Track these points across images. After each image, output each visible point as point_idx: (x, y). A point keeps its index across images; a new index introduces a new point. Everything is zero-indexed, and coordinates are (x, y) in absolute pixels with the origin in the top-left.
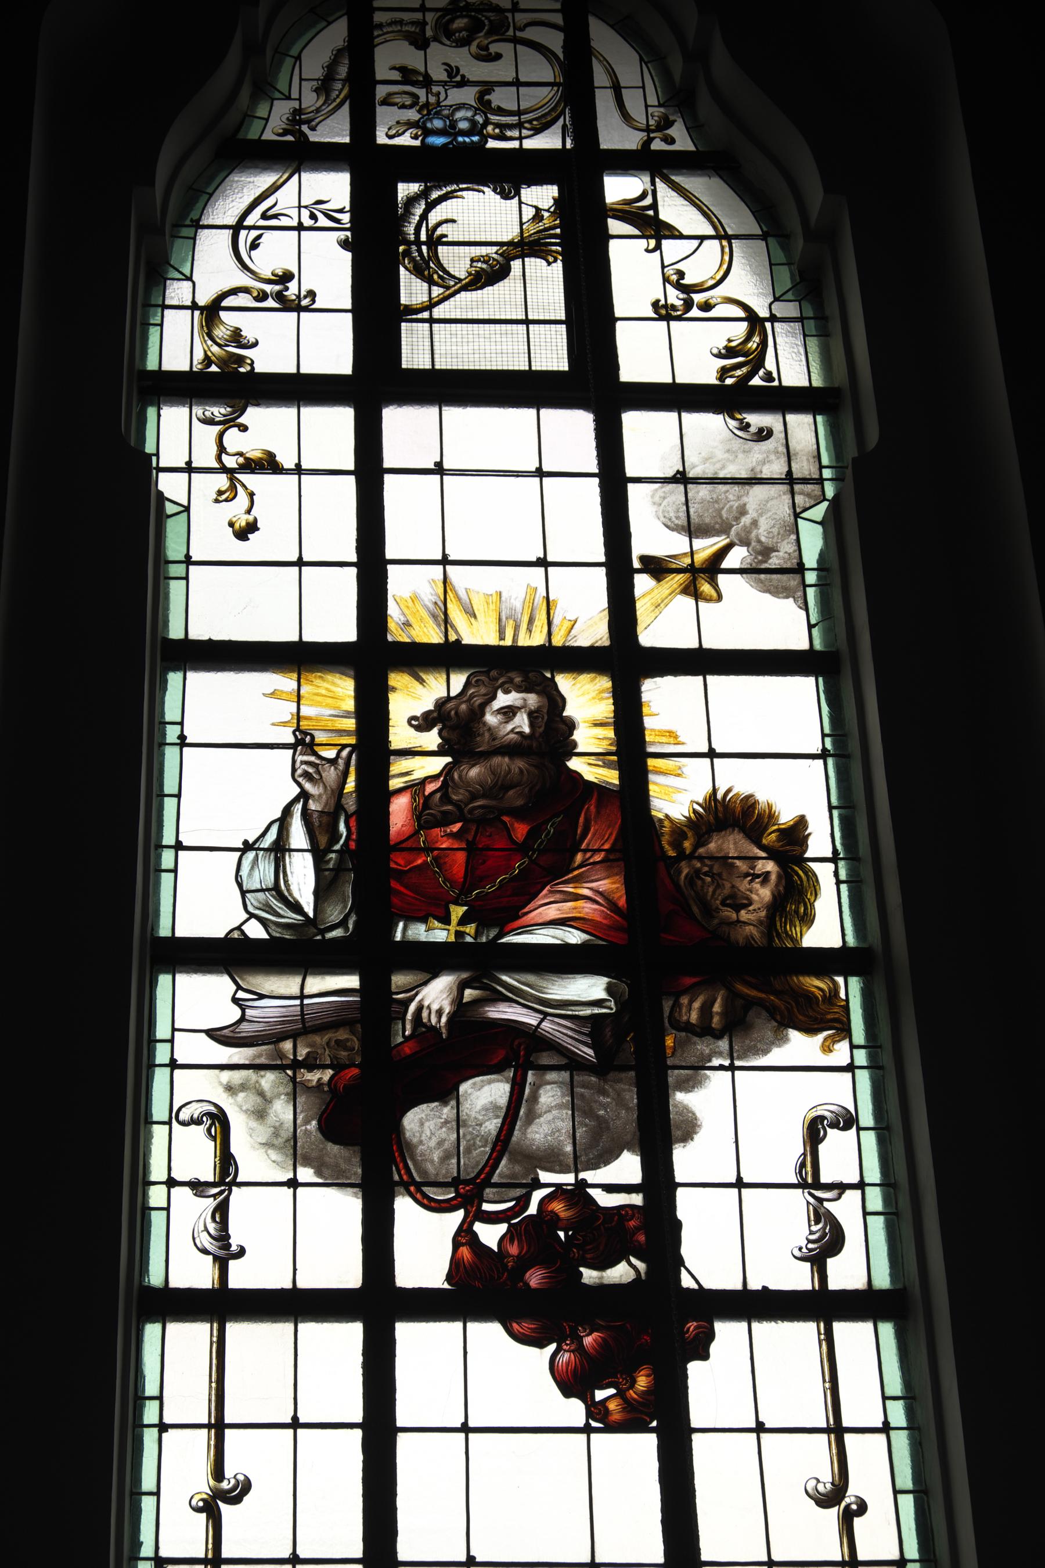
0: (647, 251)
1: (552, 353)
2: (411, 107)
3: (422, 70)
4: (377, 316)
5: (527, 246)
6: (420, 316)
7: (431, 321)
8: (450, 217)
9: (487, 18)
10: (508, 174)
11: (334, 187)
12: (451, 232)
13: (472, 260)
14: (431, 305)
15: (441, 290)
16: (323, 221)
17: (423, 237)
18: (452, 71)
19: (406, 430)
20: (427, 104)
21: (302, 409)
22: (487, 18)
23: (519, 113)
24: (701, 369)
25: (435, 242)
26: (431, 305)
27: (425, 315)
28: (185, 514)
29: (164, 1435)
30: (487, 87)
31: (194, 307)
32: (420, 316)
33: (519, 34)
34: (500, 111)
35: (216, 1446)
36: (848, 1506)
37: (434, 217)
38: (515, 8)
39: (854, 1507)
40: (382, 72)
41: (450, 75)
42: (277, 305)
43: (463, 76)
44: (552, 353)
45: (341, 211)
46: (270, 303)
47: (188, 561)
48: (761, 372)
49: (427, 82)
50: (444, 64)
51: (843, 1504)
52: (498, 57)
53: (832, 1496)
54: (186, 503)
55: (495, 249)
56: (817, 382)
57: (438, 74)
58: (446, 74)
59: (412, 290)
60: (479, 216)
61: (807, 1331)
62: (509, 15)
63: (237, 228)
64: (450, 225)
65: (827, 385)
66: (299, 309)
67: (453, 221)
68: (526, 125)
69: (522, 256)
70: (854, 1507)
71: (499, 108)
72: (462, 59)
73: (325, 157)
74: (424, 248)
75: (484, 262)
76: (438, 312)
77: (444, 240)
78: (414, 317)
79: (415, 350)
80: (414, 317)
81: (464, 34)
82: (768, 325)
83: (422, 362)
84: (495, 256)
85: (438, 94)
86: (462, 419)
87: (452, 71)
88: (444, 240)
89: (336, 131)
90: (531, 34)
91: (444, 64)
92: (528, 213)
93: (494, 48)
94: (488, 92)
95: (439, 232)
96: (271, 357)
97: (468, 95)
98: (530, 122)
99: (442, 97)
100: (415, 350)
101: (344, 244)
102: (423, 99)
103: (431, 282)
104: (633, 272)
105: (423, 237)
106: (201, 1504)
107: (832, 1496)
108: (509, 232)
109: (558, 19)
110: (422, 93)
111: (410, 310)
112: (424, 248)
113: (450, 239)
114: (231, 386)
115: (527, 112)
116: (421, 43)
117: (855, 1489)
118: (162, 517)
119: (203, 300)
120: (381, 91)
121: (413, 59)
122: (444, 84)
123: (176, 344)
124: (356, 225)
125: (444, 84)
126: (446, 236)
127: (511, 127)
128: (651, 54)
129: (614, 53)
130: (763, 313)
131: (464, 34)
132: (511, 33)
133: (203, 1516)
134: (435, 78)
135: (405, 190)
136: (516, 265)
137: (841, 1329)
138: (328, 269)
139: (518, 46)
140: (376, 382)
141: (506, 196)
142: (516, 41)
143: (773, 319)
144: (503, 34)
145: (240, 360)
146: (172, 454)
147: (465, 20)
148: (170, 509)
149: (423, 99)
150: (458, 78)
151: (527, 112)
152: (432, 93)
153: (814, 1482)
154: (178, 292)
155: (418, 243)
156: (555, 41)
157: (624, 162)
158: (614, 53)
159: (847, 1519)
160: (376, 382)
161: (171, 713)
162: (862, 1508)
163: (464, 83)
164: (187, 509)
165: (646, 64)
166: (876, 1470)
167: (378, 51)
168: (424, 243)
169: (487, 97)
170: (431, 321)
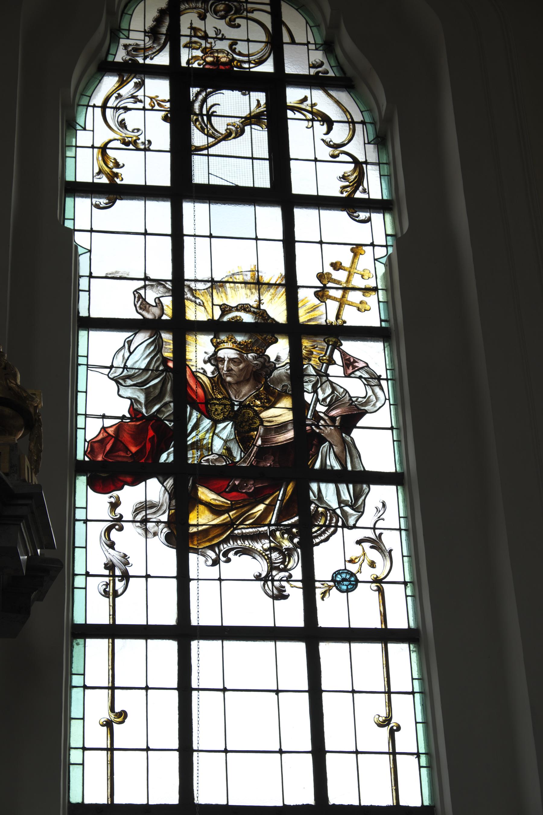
0: (307, 127)
1: (263, 180)
2: (197, 49)
3: (203, 29)
4: (182, 154)
5: (251, 119)
6: (201, 152)
7: (208, 155)
8: (217, 103)
9: (234, 5)
10: (245, 82)
11: (159, 88)
12: (218, 110)
13: (228, 125)
14: (208, 147)
15: (214, 140)
16: (157, 107)
17: (204, 112)
18: (218, 31)
19: (195, 213)
20: (206, 48)
21: (147, 202)
22: (234, 5)
23: (248, 56)
24: (332, 188)
25: (210, 116)
26: (208, 147)
27: (205, 152)
28: (89, 253)
29: (371, 241)
30: (234, 42)
31: (93, 147)
32: (201, 152)
33: (250, 15)
34: (240, 54)
35: (112, 695)
36: (392, 727)
37: (211, 101)
38: (247, 2)
39: (395, 728)
40: (185, 30)
41: (216, 34)
42: (134, 148)
43: (223, 35)
44: (263, 180)
45: (164, 101)
46: (131, 147)
47: (91, 276)
48: (361, 188)
49: (205, 37)
50: (215, 27)
51: (391, 726)
52: (239, 26)
53: (386, 722)
54: (89, 249)
55: (238, 119)
56: (385, 198)
57: (211, 33)
58: (214, 33)
59: (198, 138)
60: (231, 104)
61: (377, 647)
62: (245, 4)
63: (104, 107)
64: (217, 106)
65: (389, 198)
66: (146, 150)
67: (219, 105)
68: (252, 62)
69: (250, 124)
70: (395, 728)
71: (240, 52)
72: (222, 24)
73: (157, 72)
74: (205, 118)
75: (234, 126)
76: (212, 151)
77: (215, 114)
78: (199, 153)
79: (201, 172)
80: (199, 153)
81: (223, 13)
82: (364, 166)
83: (96, 796)
84: (238, 123)
85: (211, 43)
86: (222, 211)
87: (218, 31)
88: (215, 114)
89: (163, 59)
90: (256, 15)
91: (215, 27)
92: (254, 104)
93: (238, 21)
94: (236, 44)
95: (212, 110)
96: (130, 176)
97: (224, 45)
98: (254, 61)
99: (213, 44)
100: (201, 172)
101: (165, 119)
102: (203, 46)
103: (208, 135)
104: (301, 137)
105: (204, 112)
106: (105, 723)
107: (386, 722)
108: (245, 113)
109: (268, 8)
110: (203, 42)
111: (199, 149)
112: (205, 118)
113: (217, 114)
114: (113, 191)
115: (253, 55)
116: (202, 17)
117: (395, 720)
118: (77, 255)
119: (98, 144)
120: (184, 41)
121: (198, 24)
122: (213, 38)
123: (83, 167)
124: (172, 110)
125: (213, 38)
126: (216, 112)
127: (245, 62)
128: (313, 22)
129: (294, 21)
130: (361, 159)
131: (223, 13)
132: (245, 13)
133: (105, 728)
134: (210, 36)
135: (194, 91)
136: (247, 128)
137: (391, 646)
138: (159, 132)
139: (249, 21)
140: (182, 189)
141: (244, 94)
142: (247, 18)
143: (366, 163)
144: (242, 14)
145: (116, 175)
146: (82, 222)
147: (223, 6)
148: (80, 250)
149: (203, 46)
150: (220, 36)
151: (253, 55)
152: (209, 43)
153: (378, 716)
154: (83, 138)
155: (201, 115)
156: (267, 20)
157: (300, 81)
158: (294, 21)
159: (392, 733)
160: (182, 189)
161: (82, 351)
162: (399, 728)
163: (223, 39)
164: (90, 251)
165: (310, 27)
166: (408, 712)
167: (182, 18)
168: (205, 115)
169: (234, 47)
170: (208, 155)
